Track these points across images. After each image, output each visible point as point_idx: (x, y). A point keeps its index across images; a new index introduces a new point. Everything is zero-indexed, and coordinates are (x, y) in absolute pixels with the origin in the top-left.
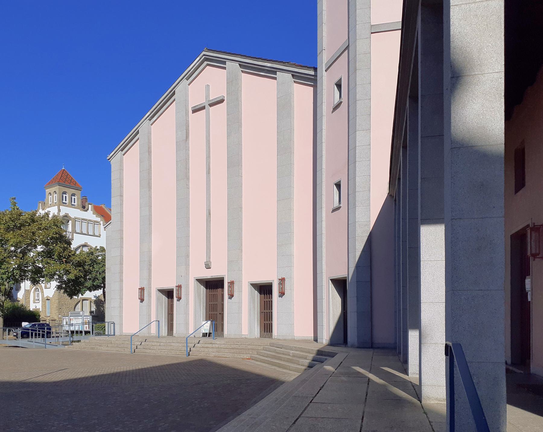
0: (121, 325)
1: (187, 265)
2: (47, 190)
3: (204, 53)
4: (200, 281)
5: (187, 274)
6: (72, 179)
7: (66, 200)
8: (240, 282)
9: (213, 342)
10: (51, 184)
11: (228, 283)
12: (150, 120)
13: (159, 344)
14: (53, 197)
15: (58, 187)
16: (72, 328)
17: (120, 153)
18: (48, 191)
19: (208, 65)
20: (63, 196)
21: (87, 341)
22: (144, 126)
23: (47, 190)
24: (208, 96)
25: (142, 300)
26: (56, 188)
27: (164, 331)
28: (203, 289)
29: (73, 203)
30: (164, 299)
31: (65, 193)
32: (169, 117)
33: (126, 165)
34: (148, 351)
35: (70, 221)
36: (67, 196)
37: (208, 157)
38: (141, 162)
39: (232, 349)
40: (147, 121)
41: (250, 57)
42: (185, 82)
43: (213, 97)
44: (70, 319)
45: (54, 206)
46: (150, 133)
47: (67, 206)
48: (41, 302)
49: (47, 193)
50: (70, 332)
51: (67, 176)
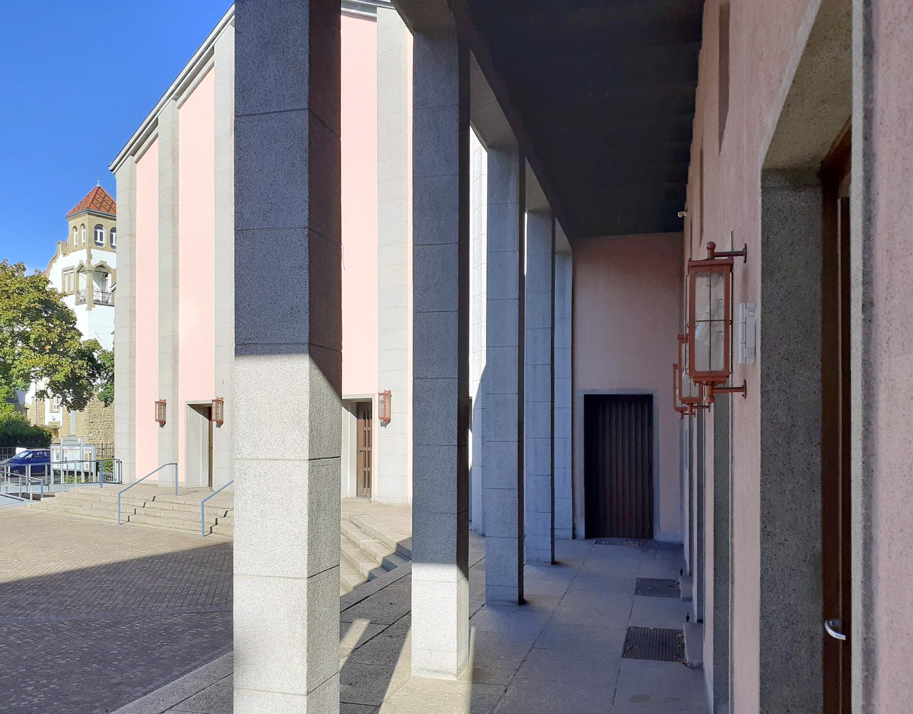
0: (132, 464)
7: (101, 239)
8: (175, 401)
10: (75, 214)
11: (380, 394)
12: (176, 99)
13: (171, 508)
15: (88, 216)
16: (65, 466)
17: (130, 160)
18: (72, 223)
20: (96, 232)
22: (166, 111)
25: (163, 424)
26: (85, 219)
27: (203, 481)
29: (114, 244)
30: (202, 419)
31: (99, 226)
34: (148, 520)
35: (109, 275)
38: (161, 174)
40: (171, 102)
46: (175, 123)
47: (103, 249)
50: (83, 474)
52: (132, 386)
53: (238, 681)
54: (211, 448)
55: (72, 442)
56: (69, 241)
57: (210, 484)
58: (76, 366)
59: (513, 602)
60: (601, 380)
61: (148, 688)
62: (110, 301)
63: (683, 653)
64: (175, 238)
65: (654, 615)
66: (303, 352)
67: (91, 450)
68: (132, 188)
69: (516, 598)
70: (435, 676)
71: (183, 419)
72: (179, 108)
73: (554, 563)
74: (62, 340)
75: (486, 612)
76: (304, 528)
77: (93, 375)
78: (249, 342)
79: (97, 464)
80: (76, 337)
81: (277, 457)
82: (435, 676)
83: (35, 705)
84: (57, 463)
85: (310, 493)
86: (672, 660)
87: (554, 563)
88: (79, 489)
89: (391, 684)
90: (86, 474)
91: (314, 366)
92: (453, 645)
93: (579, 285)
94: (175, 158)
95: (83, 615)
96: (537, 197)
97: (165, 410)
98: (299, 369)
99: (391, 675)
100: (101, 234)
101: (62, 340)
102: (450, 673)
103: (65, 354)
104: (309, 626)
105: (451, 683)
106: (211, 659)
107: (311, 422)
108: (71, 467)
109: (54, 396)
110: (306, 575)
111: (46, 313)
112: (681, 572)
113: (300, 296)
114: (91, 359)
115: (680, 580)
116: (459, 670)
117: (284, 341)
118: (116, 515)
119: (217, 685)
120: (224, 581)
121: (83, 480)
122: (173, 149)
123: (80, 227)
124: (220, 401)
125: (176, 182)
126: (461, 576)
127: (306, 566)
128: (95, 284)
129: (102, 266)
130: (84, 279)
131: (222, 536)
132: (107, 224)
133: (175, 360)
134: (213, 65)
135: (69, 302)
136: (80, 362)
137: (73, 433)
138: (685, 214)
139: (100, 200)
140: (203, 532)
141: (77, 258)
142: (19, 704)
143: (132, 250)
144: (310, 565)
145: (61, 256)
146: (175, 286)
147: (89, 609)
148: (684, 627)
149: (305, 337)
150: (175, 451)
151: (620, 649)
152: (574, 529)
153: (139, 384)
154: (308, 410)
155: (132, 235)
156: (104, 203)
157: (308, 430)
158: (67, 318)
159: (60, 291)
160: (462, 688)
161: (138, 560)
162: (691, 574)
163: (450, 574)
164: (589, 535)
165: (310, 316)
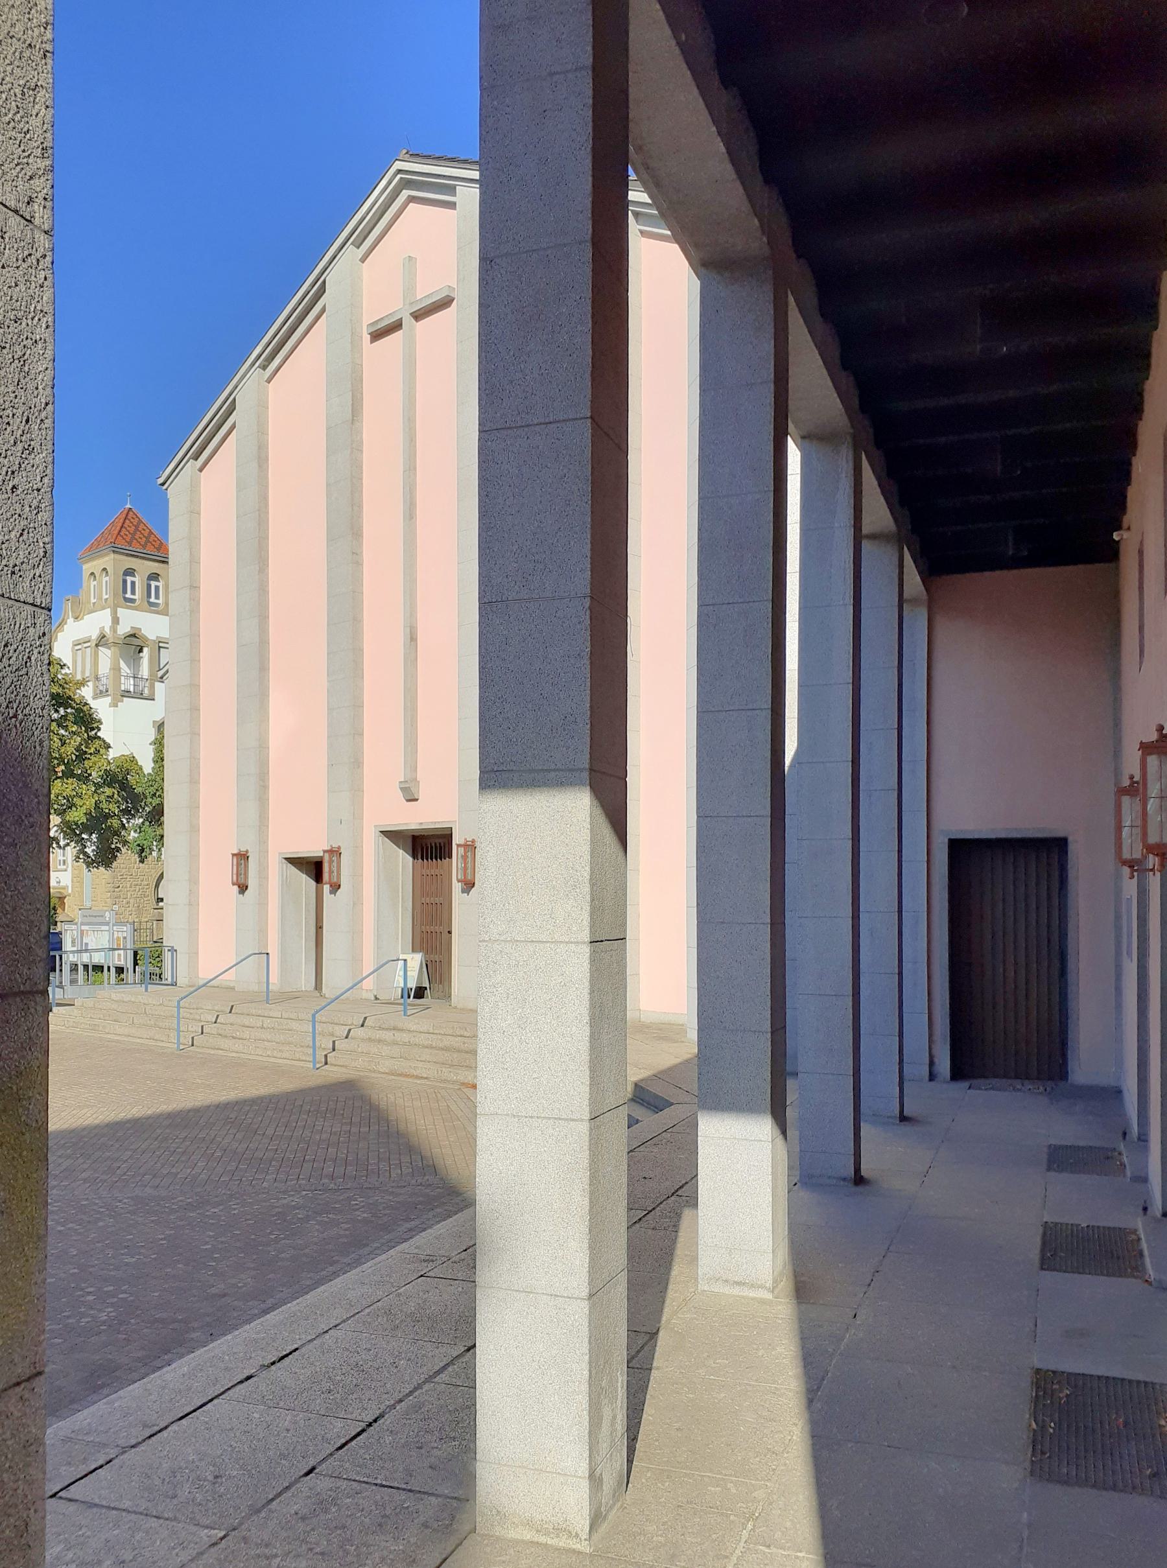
0: (194, 954)
1: (357, 790)
2: (85, 567)
3: (398, 165)
4: (392, 835)
5: (357, 815)
6: (151, 533)
7: (133, 593)
8: (264, 852)
9: (400, 1025)
10: (94, 551)
12: (264, 368)
13: (259, 1024)
14: (100, 583)
15: (112, 555)
16: (85, 958)
17: (191, 466)
18: (87, 568)
19: (412, 199)
20: (125, 582)
21: (89, 1003)
22: (249, 387)
23: (85, 567)
24: (410, 288)
25: (243, 888)
26: (108, 560)
27: (305, 982)
28: (403, 859)
29: (153, 600)
30: (305, 882)
31: (130, 572)
32: (311, 355)
33: (204, 500)
34: (225, 1043)
35: (145, 650)
36: (136, 580)
37: (410, 469)
39: (446, 1049)
40: (256, 372)
41: (428, 157)
42: (351, 253)
43: (426, 292)
44: (82, 931)
45: (103, 608)
46: (263, 405)
47: (136, 609)
48: (70, 869)
49: (86, 575)
50: (81, 968)
51: (137, 527)
52: (194, 829)
53: (483, 1276)
54: (319, 928)
55: (95, 920)
56: (82, 595)
57: (318, 985)
58: (102, 798)
59: (844, 1179)
60: (973, 813)
61: (270, 1302)
62: (146, 691)
63: (1143, 1264)
64: (263, 590)
65: (1082, 1203)
66: (581, 784)
67: (125, 932)
68: (194, 512)
69: (851, 1172)
70: (736, 1291)
71: (276, 881)
72: (269, 381)
73: (903, 1118)
74: (81, 756)
75: (803, 1194)
76: (584, 1046)
77: (126, 812)
78: (500, 770)
79: (136, 954)
80: (102, 751)
81: (543, 937)
82: (736, 1291)
83: (104, 1322)
84: (73, 952)
85: (592, 992)
86: (1126, 1276)
87: (903, 1118)
88: (110, 993)
89: (668, 1302)
90: (120, 970)
91: (595, 802)
92: (767, 1242)
93: (938, 654)
94: (262, 461)
95: (148, 1190)
96: (878, 513)
97: (246, 867)
98: (577, 806)
99: (666, 1288)
100: (133, 583)
101: (81, 756)
102: (761, 1287)
103: (85, 778)
104: (592, 1193)
105: (762, 1302)
106: (358, 1262)
107: (592, 885)
108: (98, 959)
109: (68, 844)
110: (587, 1116)
111: (57, 711)
112: (1125, 1134)
113: (580, 700)
114: (124, 786)
115: (1122, 1147)
116: (775, 1281)
117: (553, 767)
118: (173, 1034)
119: (399, 1295)
120: (272, 1159)
121: (113, 979)
122: (259, 448)
123: (99, 572)
124: (335, 852)
125: (264, 498)
126: (777, 1132)
127: (586, 1102)
128: (122, 664)
129: (134, 636)
130: (106, 657)
131: (343, 1070)
132: (146, 567)
133: (263, 787)
134: (323, 310)
135: (87, 693)
136: (108, 791)
137: (88, 904)
138: (1126, 535)
139: (132, 529)
140: (314, 1062)
141: (96, 623)
142: (79, 1321)
143: (194, 611)
144: (593, 1102)
145: (70, 620)
146: (263, 668)
147: (158, 1181)
148: (1139, 1224)
149: (584, 761)
150: (263, 932)
151: (1035, 1255)
152: (932, 1063)
153: (204, 823)
154: (588, 869)
155: (194, 587)
156: (138, 534)
157: (588, 898)
158: (86, 720)
159: (79, 677)
160: (783, 1310)
161: (218, 1106)
162: (1143, 1138)
163: (762, 1128)
164: (958, 1074)
165: (591, 730)
